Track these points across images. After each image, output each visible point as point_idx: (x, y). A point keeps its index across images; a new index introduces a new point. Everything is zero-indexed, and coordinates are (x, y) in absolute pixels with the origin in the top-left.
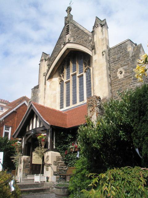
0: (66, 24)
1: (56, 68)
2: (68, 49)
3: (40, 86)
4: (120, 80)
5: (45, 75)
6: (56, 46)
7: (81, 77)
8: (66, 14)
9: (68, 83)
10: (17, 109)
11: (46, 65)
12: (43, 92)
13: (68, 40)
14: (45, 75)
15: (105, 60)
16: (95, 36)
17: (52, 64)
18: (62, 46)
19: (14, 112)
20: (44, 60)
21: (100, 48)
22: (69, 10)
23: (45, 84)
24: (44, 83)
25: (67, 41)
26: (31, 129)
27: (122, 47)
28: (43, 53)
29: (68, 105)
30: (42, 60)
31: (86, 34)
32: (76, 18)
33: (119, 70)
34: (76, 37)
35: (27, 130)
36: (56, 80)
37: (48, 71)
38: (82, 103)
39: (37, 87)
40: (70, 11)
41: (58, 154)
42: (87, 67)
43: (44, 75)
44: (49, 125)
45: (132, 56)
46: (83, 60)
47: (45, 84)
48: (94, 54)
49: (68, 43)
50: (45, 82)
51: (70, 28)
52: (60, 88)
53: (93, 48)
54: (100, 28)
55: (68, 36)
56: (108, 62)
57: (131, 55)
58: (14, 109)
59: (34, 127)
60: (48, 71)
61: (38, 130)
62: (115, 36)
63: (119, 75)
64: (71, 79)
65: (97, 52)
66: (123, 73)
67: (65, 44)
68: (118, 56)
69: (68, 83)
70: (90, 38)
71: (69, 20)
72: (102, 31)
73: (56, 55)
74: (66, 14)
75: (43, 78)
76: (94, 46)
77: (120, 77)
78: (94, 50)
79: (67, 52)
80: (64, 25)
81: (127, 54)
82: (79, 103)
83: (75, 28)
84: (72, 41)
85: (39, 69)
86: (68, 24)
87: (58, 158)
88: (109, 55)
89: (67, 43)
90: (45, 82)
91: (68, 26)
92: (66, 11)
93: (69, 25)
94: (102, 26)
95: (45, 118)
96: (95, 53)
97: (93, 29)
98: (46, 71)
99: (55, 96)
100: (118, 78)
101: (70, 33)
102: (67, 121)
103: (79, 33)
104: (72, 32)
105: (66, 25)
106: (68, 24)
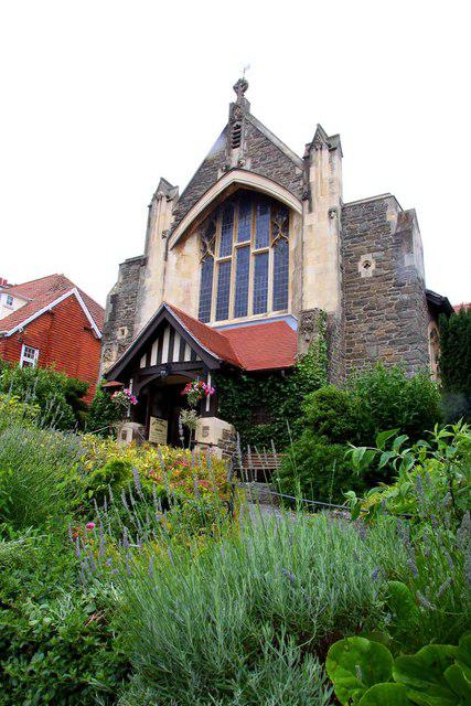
0: (232, 121)
1: (198, 223)
2: (234, 183)
3: (150, 261)
4: (363, 281)
5: (166, 236)
6: (200, 169)
7: (262, 256)
8: (234, 98)
9: (225, 264)
10: (54, 308)
11: (169, 212)
12: (160, 277)
13: (239, 162)
14: (166, 236)
15: (334, 230)
16: (312, 169)
17: (187, 212)
18: (220, 174)
19: (47, 313)
20: (165, 199)
21: (323, 202)
22: (241, 87)
23: (166, 259)
24: (162, 256)
25: (234, 164)
26: (153, 362)
27: (373, 209)
28: (162, 179)
29: (222, 315)
30: (157, 198)
31: (289, 159)
32: (262, 110)
33: (364, 258)
34: (261, 160)
35: (143, 365)
36: (193, 248)
37: (175, 227)
38: (237, 320)
39: (141, 262)
40: (244, 91)
41: (227, 426)
42: (281, 233)
43: (164, 237)
44: (218, 361)
45: (396, 234)
46: (269, 216)
47: (166, 259)
48: (306, 210)
49: (239, 168)
50: (167, 254)
51: (245, 133)
52: (200, 274)
53: (306, 197)
54: (326, 153)
55: (237, 154)
56: (342, 236)
57: (393, 231)
58: (49, 307)
59: (165, 360)
60: (175, 227)
61: (174, 368)
62: (357, 180)
63: (361, 268)
64: (233, 256)
65: (316, 206)
66: (373, 267)
67: (228, 171)
68: (364, 226)
69: (225, 264)
70: (298, 171)
71: (239, 112)
72: (330, 162)
73: (202, 193)
74: (234, 98)
75: (159, 245)
76: (309, 192)
77: (366, 273)
78: (307, 202)
79: (231, 191)
80: (226, 121)
81: (385, 226)
82: (251, 317)
83: (257, 136)
84: (248, 166)
85: (150, 219)
86: (238, 123)
87: (225, 434)
88: (342, 220)
89: (234, 169)
90: (167, 254)
91: (239, 127)
92: (234, 88)
93: (239, 127)
94: (332, 150)
95: (205, 345)
96: (310, 210)
97: (309, 151)
98: (168, 227)
99: (188, 292)
100: (359, 274)
101: (244, 145)
102: (431, 351)
103: (268, 151)
104: (249, 144)
105: (232, 124)
106: (238, 123)
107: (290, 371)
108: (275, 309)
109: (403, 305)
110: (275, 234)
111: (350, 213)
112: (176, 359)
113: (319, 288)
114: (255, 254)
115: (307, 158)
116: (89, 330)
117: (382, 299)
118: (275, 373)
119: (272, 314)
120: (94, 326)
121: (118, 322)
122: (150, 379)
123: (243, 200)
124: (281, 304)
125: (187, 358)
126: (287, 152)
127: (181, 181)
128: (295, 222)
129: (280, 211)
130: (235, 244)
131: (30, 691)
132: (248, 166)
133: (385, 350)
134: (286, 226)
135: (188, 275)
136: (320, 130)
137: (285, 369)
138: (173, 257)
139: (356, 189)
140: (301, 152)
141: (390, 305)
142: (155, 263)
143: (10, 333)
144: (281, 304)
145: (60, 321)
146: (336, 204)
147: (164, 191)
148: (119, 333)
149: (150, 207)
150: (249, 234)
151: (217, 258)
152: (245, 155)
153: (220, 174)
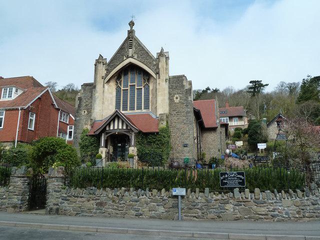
11: (104, 69)
19: (39, 98)
21: (163, 76)
22: (132, 24)
24: (102, 86)
32: (140, 35)
33: (176, 96)
37: (107, 75)
38: (131, 112)
48: (158, 77)
49: (132, 57)
53: (158, 73)
58: (39, 96)
60: (107, 75)
62: (174, 70)
63: (175, 99)
64: (129, 88)
65: (161, 77)
66: (179, 99)
67: (128, 57)
77: (177, 101)
96: (159, 78)
98: (104, 75)
103: (143, 52)
107: (158, 133)
108: (144, 109)
109: (188, 112)
110: (144, 82)
111: (172, 80)
112: (116, 128)
113: (162, 106)
114: (137, 89)
115: (158, 58)
116: (53, 105)
117: (181, 110)
118: (153, 134)
119: (144, 111)
120: (55, 103)
121: (82, 108)
122: (111, 134)
123: (131, 68)
124: (147, 107)
125: (125, 128)
126: (150, 55)
127: (108, 57)
128: (152, 80)
129: (147, 76)
130: (129, 84)
131: (300, 162)
132: (136, 57)
133: (182, 126)
134: (148, 80)
135: (111, 93)
136: (162, 50)
137: (156, 132)
138: (106, 86)
139: (174, 72)
140: (155, 56)
141: (184, 112)
142: (99, 87)
143: (26, 107)
144: (147, 107)
145: (45, 104)
146: (168, 77)
147: (100, 61)
148: (83, 112)
149: (95, 65)
150: (134, 81)
151: (122, 88)
152: (135, 53)
153: (125, 58)
